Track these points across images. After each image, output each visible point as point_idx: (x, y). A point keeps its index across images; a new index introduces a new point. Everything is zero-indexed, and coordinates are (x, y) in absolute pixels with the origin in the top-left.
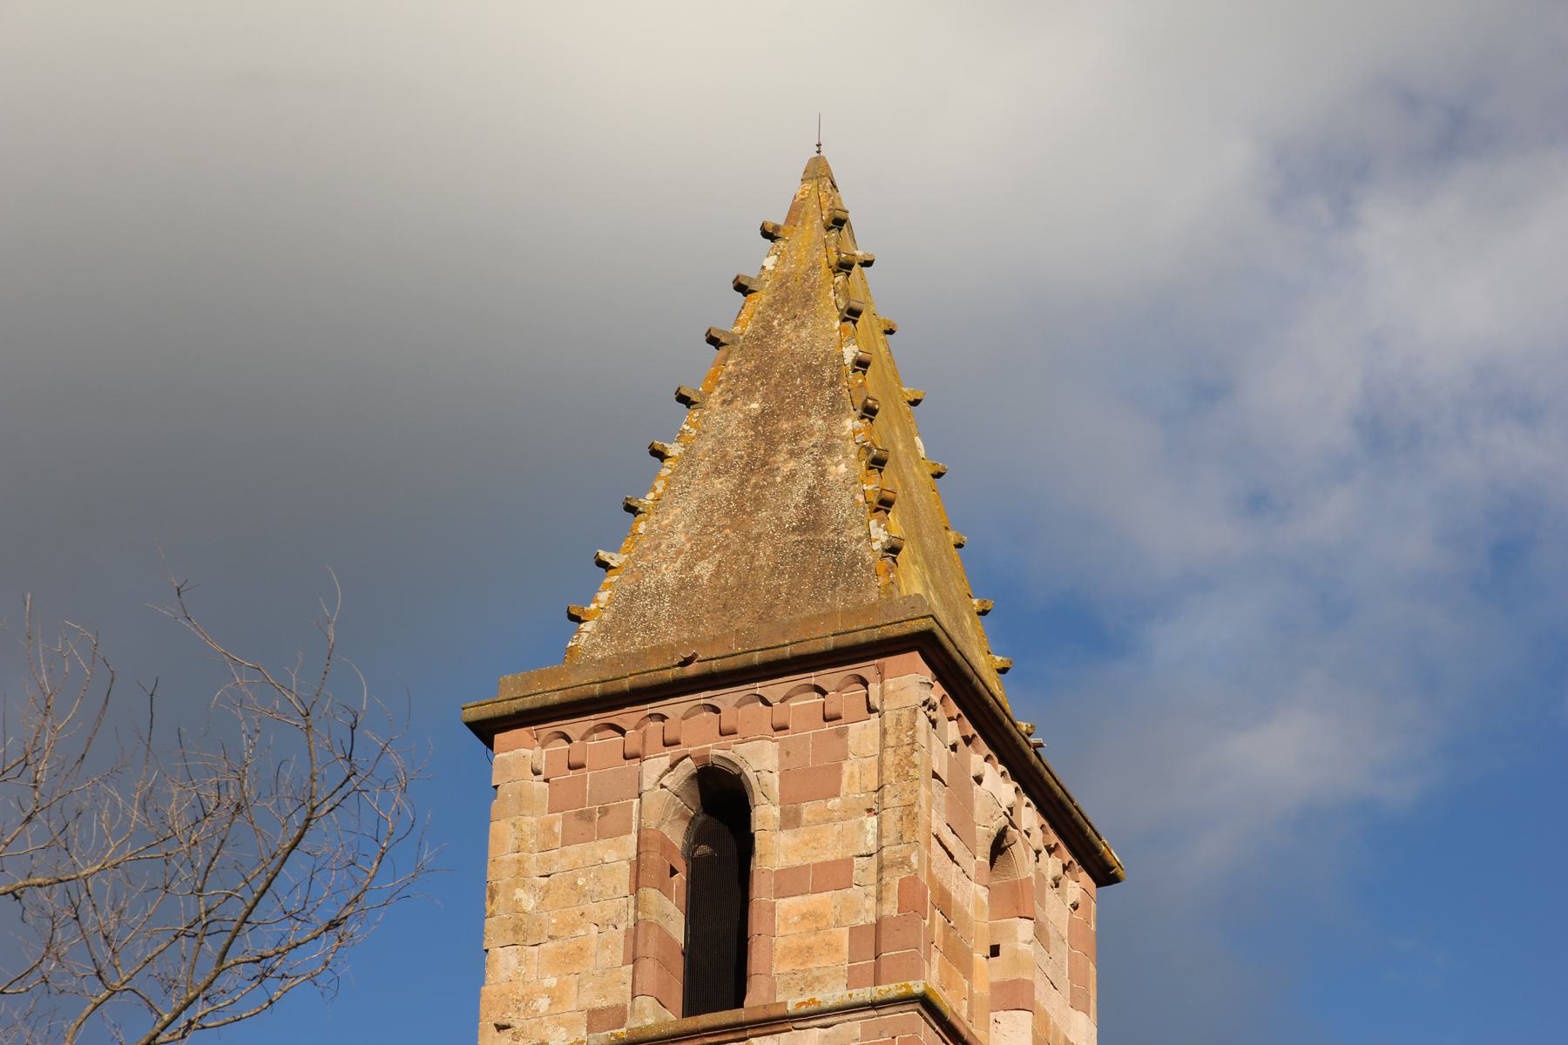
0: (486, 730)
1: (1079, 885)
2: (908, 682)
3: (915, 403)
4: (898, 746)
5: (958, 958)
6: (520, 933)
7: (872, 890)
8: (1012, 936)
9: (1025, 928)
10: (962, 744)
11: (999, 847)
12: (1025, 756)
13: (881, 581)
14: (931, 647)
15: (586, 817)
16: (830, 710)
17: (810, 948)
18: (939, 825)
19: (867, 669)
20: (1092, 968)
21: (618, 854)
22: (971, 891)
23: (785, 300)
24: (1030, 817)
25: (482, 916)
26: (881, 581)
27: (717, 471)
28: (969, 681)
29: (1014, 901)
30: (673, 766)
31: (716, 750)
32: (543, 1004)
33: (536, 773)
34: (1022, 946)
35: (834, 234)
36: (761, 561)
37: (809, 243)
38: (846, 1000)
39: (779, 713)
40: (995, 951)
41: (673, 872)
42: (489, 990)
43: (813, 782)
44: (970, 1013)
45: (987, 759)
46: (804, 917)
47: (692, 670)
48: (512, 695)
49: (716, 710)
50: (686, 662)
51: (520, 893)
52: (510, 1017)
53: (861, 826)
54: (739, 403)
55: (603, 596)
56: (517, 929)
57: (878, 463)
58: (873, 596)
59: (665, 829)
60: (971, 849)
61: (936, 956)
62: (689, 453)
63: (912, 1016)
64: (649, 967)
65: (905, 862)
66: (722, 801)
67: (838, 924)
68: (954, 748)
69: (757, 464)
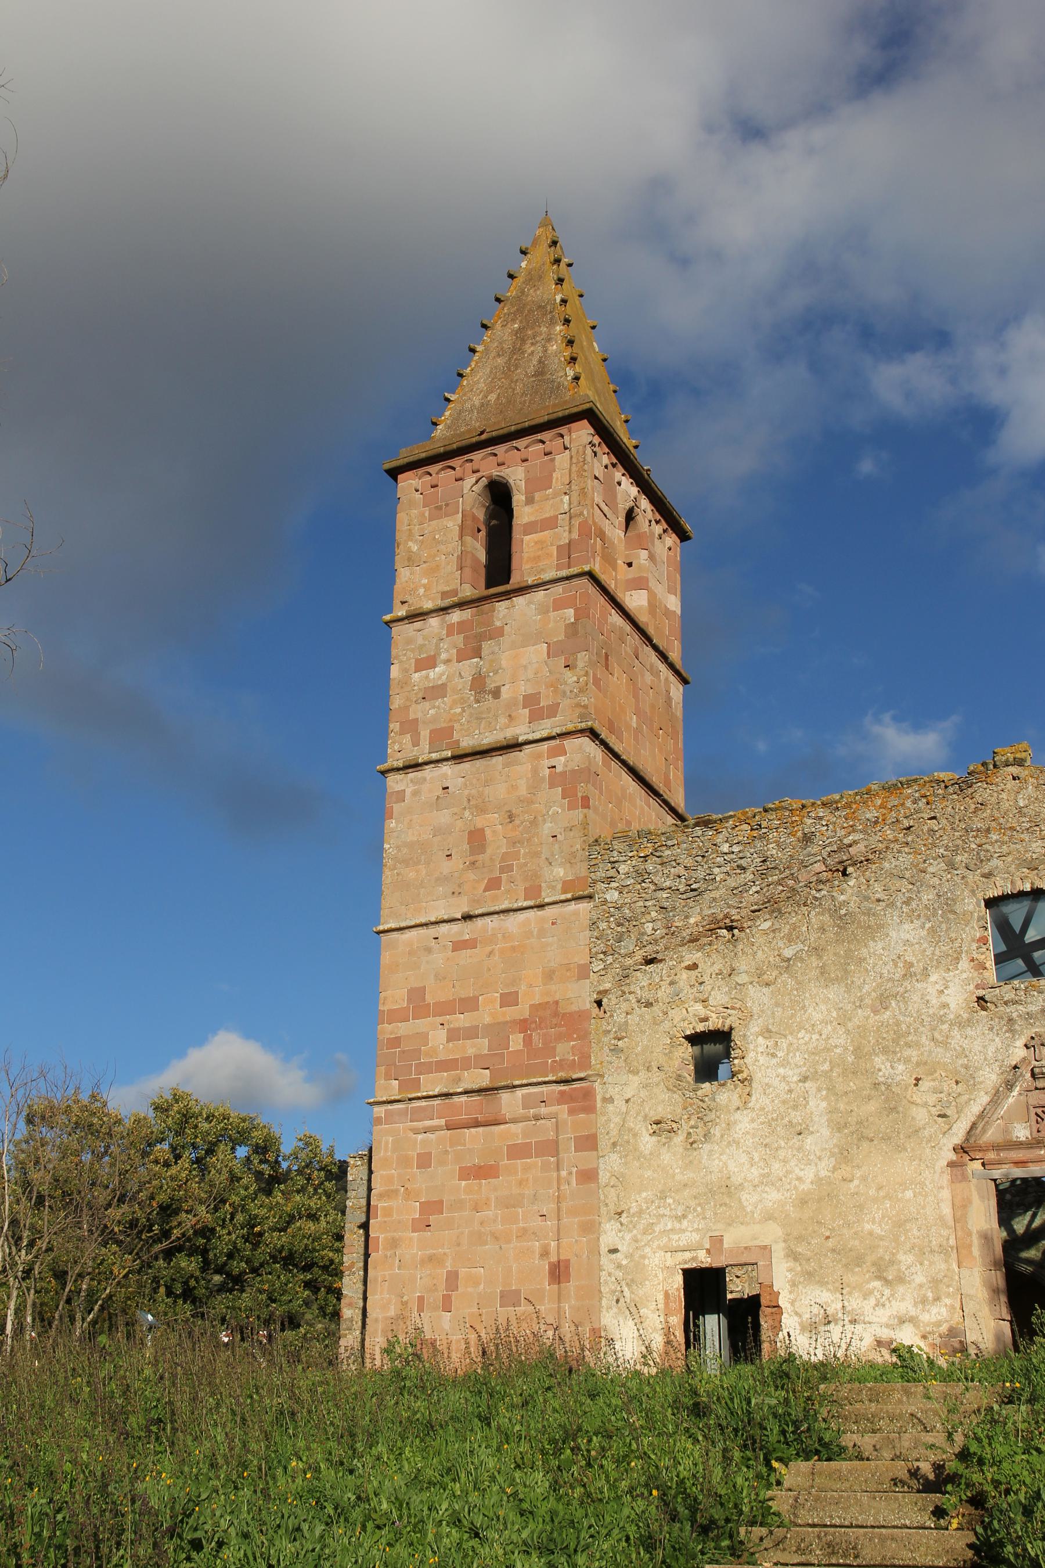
0: (393, 473)
1: (671, 540)
2: (582, 433)
3: (593, 328)
4: (578, 463)
5: (609, 560)
6: (411, 561)
7: (567, 528)
8: (638, 557)
9: (644, 554)
10: (610, 466)
11: (630, 516)
12: (642, 475)
13: (571, 393)
14: (590, 416)
15: (439, 508)
16: (547, 450)
17: (539, 557)
18: (598, 499)
19: (563, 430)
20: (678, 577)
21: (453, 524)
22: (616, 532)
23: (531, 279)
24: (645, 503)
25: (393, 555)
26: (571, 393)
27: (499, 356)
28: (612, 435)
29: (642, 542)
30: (477, 482)
31: (496, 472)
32: (422, 591)
33: (417, 491)
34: (643, 562)
35: (553, 248)
36: (518, 390)
37: (542, 254)
38: (555, 577)
39: (523, 454)
40: (630, 565)
41: (479, 531)
42: (397, 587)
43: (539, 483)
44: (616, 586)
45: (623, 475)
46: (536, 543)
47: (484, 437)
48: (405, 455)
49: (495, 455)
50: (482, 433)
51: (410, 544)
52: (407, 598)
53: (562, 500)
54: (509, 325)
55: (447, 413)
56: (409, 559)
57: (570, 342)
58: (567, 398)
59: (474, 511)
60: (616, 513)
61: (598, 559)
62: (487, 350)
63: (585, 581)
64: (467, 571)
65: (582, 514)
66: (499, 495)
67: (552, 545)
68: (606, 467)
69: (517, 351)
